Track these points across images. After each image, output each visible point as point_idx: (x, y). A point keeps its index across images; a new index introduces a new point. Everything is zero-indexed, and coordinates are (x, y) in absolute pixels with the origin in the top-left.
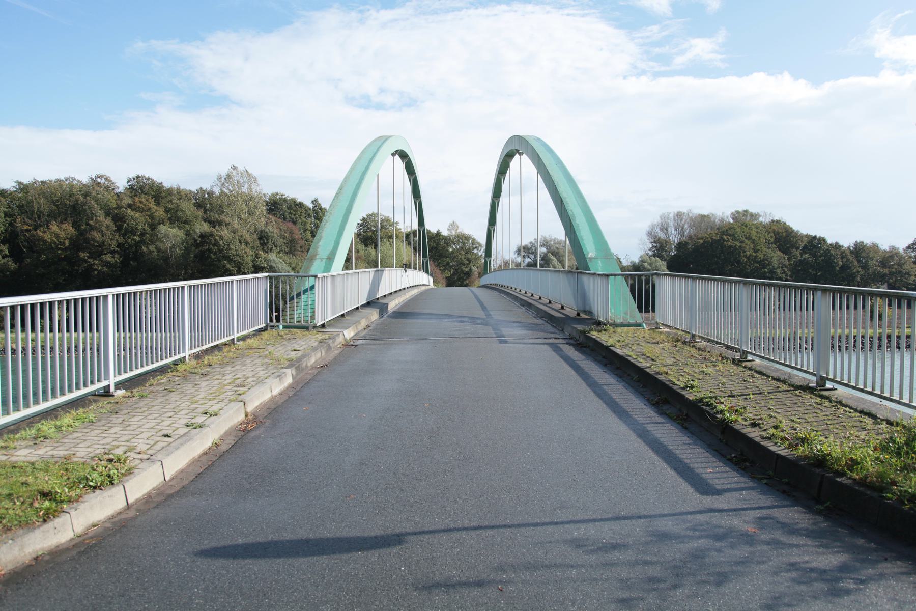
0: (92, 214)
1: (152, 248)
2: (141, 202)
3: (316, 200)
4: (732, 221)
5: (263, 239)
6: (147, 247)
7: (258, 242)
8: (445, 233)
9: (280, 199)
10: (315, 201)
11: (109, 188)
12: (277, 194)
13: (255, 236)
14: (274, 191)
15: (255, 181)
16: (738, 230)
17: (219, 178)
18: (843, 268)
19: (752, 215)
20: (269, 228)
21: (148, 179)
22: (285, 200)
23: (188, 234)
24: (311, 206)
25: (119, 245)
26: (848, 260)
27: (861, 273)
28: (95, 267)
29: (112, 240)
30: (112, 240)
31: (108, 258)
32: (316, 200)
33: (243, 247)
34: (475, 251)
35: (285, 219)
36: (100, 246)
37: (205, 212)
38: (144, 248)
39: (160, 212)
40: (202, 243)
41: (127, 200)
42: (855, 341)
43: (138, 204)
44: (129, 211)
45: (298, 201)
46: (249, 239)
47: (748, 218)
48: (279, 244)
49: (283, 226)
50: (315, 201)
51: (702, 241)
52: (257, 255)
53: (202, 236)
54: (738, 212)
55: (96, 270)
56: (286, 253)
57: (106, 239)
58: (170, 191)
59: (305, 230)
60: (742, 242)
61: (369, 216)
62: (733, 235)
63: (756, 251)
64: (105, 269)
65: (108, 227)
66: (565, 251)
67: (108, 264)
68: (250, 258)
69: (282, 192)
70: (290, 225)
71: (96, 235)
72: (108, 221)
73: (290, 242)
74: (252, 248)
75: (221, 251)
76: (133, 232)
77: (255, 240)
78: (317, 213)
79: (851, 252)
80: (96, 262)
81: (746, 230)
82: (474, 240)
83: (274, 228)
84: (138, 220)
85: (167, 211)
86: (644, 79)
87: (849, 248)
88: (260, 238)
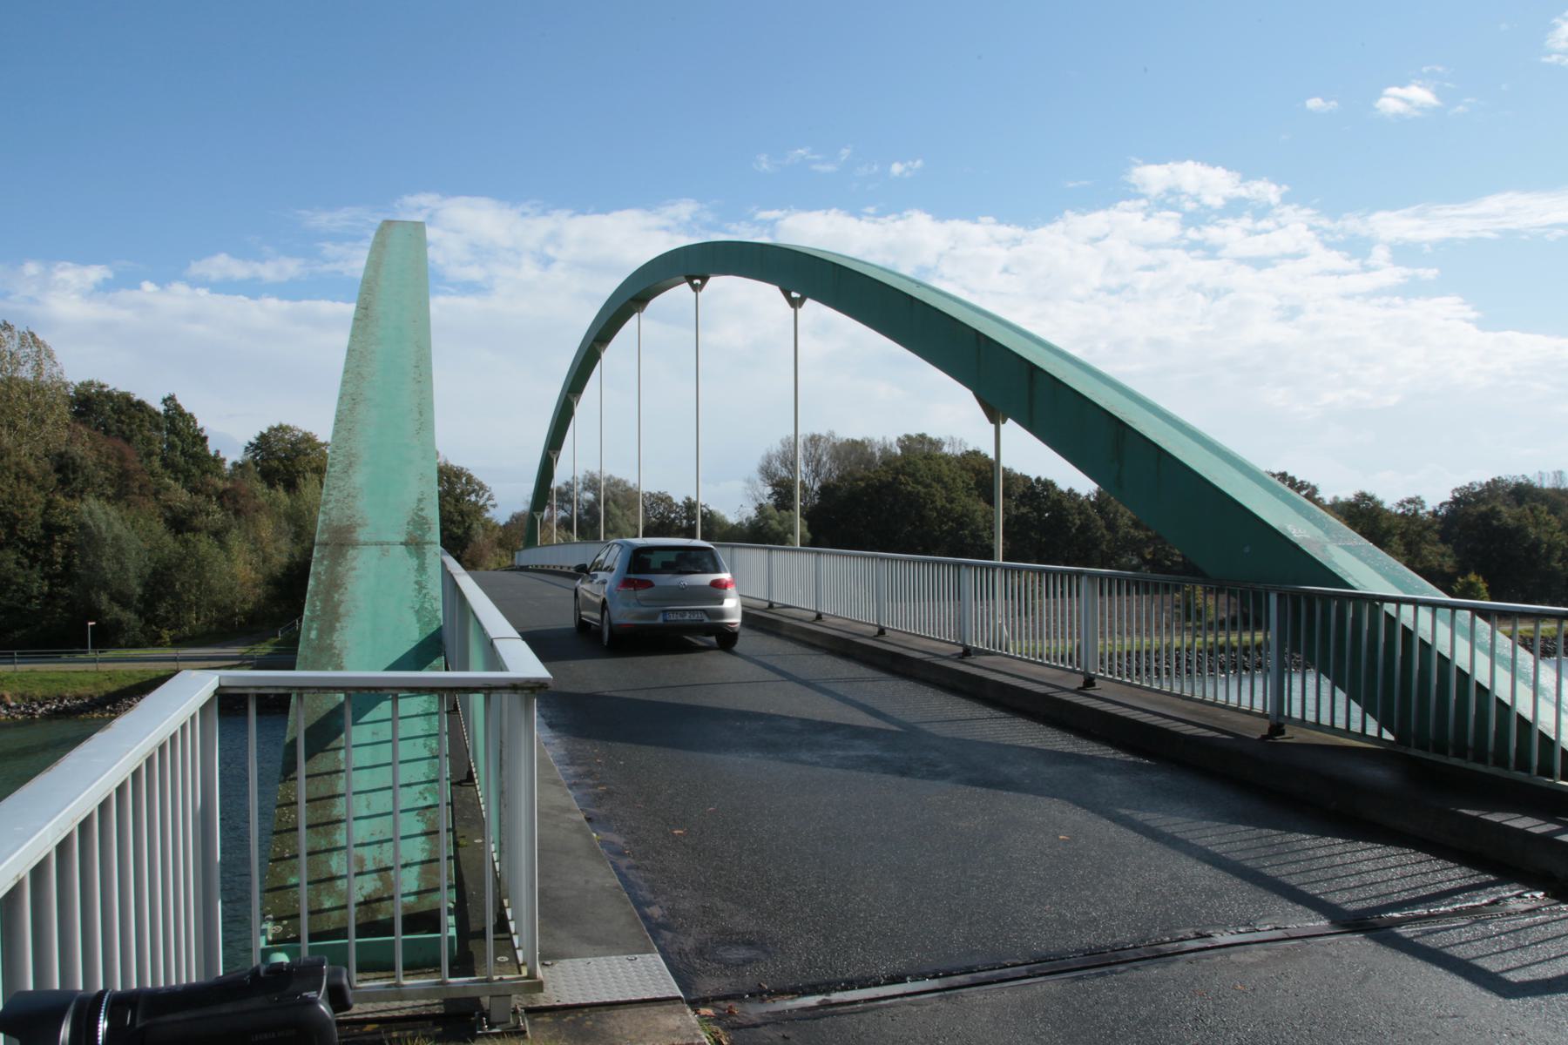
3: (1560, 473)
4: (899, 451)
5: (65, 467)
9: (99, 394)
10: (169, 400)
12: (91, 384)
13: (46, 464)
14: (86, 379)
15: (50, 356)
16: (921, 464)
18: (1084, 528)
19: (931, 442)
20: (78, 450)
22: (109, 396)
24: (161, 408)
26: (1089, 516)
27: (1108, 537)
33: (24, 486)
34: (473, 498)
35: (107, 432)
42: (1178, 659)
45: (136, 398)
46: (33, 470)
47: (926, 447)
48: (98, 480)
49: (107, 446)
50: (169, 400)
51: (862, 484)
52: (50, 504)
54: (908, 437)
56: (108, 499)
59: (150, 454)
60: (927, 486)
62: (912, 475)
63: (951, 501)
66: (991, 527)
68: (38, 509)
69: (103, 381)
70: (120, 443)
73: (120, 476)
77: (46, 474)
79: (1092, 504)
81: (933, 465)
82: (470, 479)
83: (84, 448)
86: (1311, 235)
87: (1088, 497)
88: (59, 469)
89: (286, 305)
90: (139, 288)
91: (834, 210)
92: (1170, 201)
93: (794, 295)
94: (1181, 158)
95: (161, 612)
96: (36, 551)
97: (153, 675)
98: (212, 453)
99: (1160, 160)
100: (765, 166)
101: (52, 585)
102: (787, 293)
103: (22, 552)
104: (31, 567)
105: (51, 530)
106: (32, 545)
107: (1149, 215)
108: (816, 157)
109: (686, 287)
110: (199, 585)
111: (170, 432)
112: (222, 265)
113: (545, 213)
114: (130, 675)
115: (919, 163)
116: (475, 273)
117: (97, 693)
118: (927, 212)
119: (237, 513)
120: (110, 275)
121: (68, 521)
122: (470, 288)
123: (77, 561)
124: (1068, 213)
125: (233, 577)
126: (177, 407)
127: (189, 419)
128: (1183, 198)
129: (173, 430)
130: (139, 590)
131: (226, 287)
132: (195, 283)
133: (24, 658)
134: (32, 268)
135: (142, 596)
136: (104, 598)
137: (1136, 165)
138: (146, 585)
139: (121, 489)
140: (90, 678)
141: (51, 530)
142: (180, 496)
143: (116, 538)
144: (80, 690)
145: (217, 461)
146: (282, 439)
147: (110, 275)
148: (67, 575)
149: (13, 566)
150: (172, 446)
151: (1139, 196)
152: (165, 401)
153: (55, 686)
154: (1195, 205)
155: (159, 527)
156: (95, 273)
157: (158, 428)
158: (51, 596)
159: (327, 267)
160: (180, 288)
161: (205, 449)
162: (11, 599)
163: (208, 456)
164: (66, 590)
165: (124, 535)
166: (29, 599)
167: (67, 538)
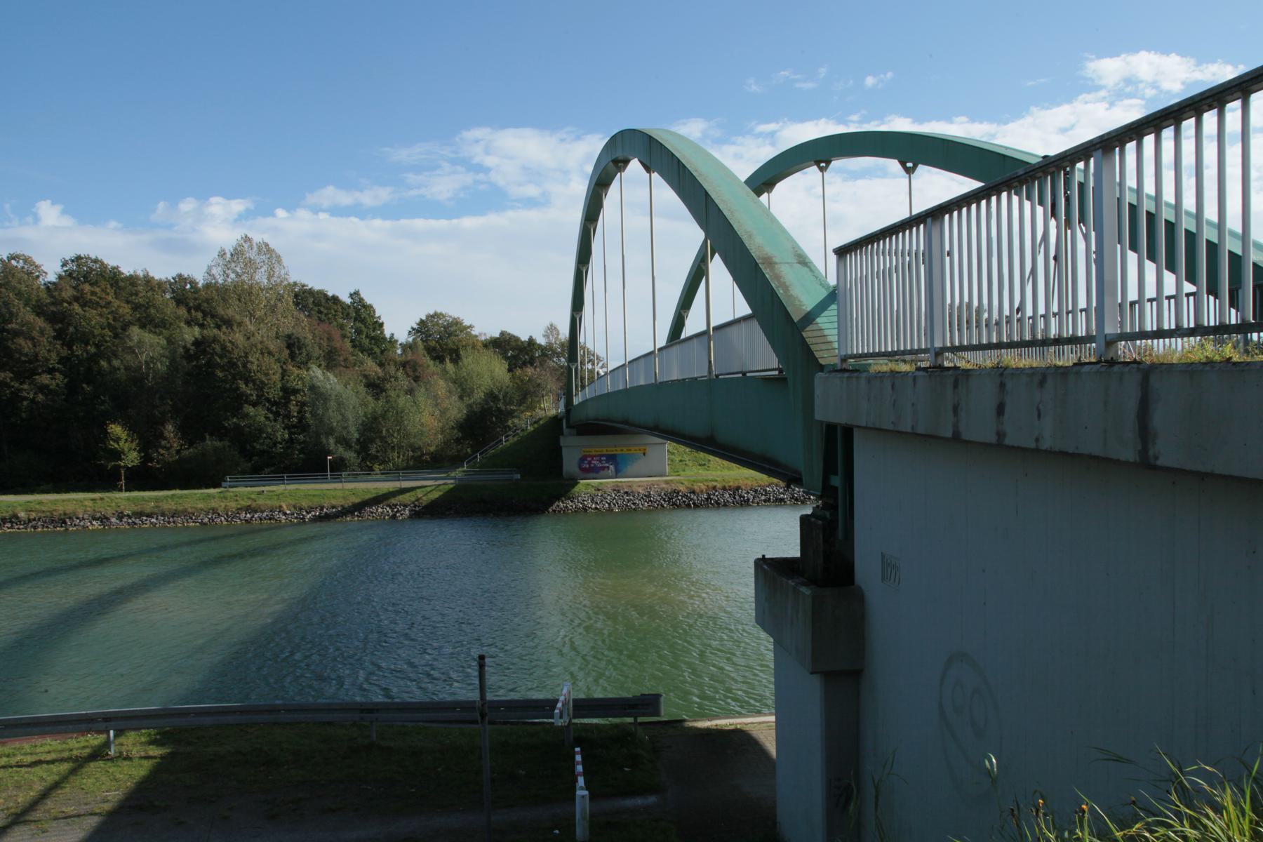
0: (11, 314)
1: (116, 363)
2: (93, 293)
3: (357, 293)
5: (293, 345)
6: (109, 362)
7: (287, 352)
8: (541, 341)
10: (355, 295)
11: (31, 270)
13: (283, 345)
17: (222, 254)
21: (96, 261)
23: (170, 341)
24: (348, 301)
25: (62, 360)
28: (25, 394)
29: (48, 349)
30: (48, 349)
31: (45, 379)
32: (357, 293)
36: (30, 362)
37: (189, 311)
38: (103, 363)
39: (125, 310)
40: (195, 357)
41: (68, 293)
43: (89, 297)
44: (76, 307)
45: (330, 294)
46: (272, 347)
50: (355, 295)
53: (197, 343)
55: (26, 399)
57: (43, 352)
58: (132, 280)
61: (430, 317)
64: (40, 397)
65: (42, 332)
67: (43, 389)
69: (304, 281)
71: (25, 345)
72: (40, 322)
74: (278, 360)
75: (232, 364)
76: (85, 339)
77: (280, 351)
78: (357, 311)
80: (25, 387)
84: (93, 319)
85: (136, 307)
88: (289, 346)
89: (388, 224)
90: (274, 215)
91: (823, 120)
92: (1128, 89)
93: (909, 165)
94: (1135, 50)
95: (373, 451)
96: (278, 407)
97: (385, 491)
98: (388, 335)
99: (1113, 54)
100: (754, 88)
101: (290, 434)
102: (903, 164)
103: (268, 409)
104: (275, 420)
105: (288, 392)
106: (275, 403)
107: (1112, 104)
108: (798, 76)
109: (815, 168)
110: (399, 431)
111: (355, 319)
112: (330, 194)
113: (578, 138)
114: (368, 491)
115: (890, 75)
116: (532, 191)
117: (347, 504)
118: (906, 116)
119: (416, 379)
120: (251, 206)
121: (300, 386)
122: (530, 203)
123: (308, 415)
124: (1034, 109)
125: (422, 425)
126: (361, 300)
127: (369, 308)
128: (1141, 86)
129: (358, 318)
130: (356, 435)
131: (337, 211)
132: (316, 210)
133: (293, 480)
134: (188, 205)
135: (358, 440)
136: (332, 441)
137: (1091, 60)
138: (361, 434)
139: (331, 360)
140: (339, 493)
141: (288, 392)
142: (371, 366)
143: (338, 396)
144: (334, 502)
145: (392, 342)
146: (437, 324)
147: (251, 206)
148: (302, 426)
149: (263, 419)
150: (359, 332)
151: (1098, 88)
152: (351, 295)
153: (316, 499)
154: (1154, 92)
155: (362, 389)
156: (238, 206)
157: (347, 316)
158: (291, 441)
159: (414, 192)
160: (303, 213)
161: (382, 333)
162: (262, 444)
163: (385, 339)
164: (301, 437)
165: (340, 392)
166: (275, 444)
167: (299, 398)
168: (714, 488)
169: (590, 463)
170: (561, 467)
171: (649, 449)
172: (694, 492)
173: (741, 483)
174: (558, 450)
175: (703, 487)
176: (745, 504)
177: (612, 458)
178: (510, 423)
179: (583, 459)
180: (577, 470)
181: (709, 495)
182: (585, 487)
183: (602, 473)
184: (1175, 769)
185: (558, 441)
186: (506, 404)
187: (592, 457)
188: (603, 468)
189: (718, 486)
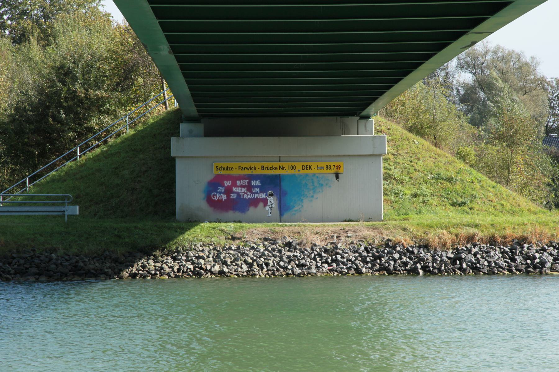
168: (471, 239)
169: (228, 191)
170: (173, 200)
171: (347, 168)
172: (426, 247)
173: (528, 231)
174: (168, 166)
175: (448, 238)
176: (534, 269)
177: (272, 183)
178: (94, 123)
179: (215, 184)
180: (204, 205)
181: (457, 252)
182: (204, 237)
183: (252, 211)
184: (381, 222)
185: (168, 147)
186: (86, 84)
187: (234, 179)
188: (255, 202)
189: (480, 234)
